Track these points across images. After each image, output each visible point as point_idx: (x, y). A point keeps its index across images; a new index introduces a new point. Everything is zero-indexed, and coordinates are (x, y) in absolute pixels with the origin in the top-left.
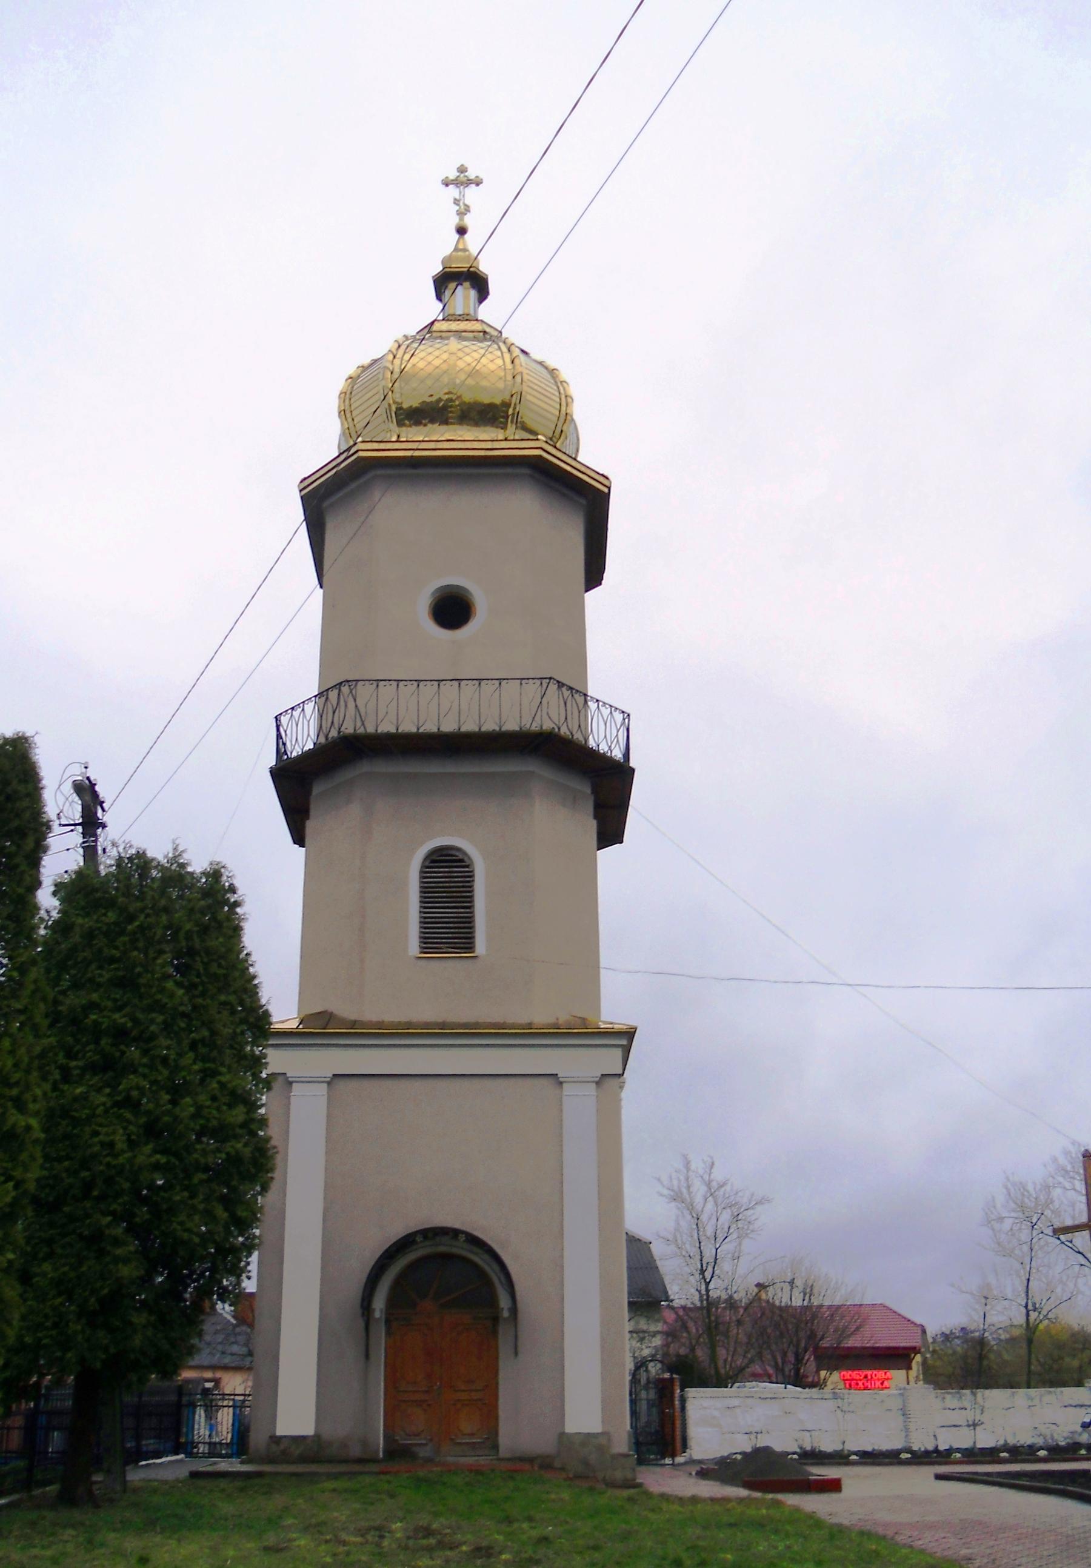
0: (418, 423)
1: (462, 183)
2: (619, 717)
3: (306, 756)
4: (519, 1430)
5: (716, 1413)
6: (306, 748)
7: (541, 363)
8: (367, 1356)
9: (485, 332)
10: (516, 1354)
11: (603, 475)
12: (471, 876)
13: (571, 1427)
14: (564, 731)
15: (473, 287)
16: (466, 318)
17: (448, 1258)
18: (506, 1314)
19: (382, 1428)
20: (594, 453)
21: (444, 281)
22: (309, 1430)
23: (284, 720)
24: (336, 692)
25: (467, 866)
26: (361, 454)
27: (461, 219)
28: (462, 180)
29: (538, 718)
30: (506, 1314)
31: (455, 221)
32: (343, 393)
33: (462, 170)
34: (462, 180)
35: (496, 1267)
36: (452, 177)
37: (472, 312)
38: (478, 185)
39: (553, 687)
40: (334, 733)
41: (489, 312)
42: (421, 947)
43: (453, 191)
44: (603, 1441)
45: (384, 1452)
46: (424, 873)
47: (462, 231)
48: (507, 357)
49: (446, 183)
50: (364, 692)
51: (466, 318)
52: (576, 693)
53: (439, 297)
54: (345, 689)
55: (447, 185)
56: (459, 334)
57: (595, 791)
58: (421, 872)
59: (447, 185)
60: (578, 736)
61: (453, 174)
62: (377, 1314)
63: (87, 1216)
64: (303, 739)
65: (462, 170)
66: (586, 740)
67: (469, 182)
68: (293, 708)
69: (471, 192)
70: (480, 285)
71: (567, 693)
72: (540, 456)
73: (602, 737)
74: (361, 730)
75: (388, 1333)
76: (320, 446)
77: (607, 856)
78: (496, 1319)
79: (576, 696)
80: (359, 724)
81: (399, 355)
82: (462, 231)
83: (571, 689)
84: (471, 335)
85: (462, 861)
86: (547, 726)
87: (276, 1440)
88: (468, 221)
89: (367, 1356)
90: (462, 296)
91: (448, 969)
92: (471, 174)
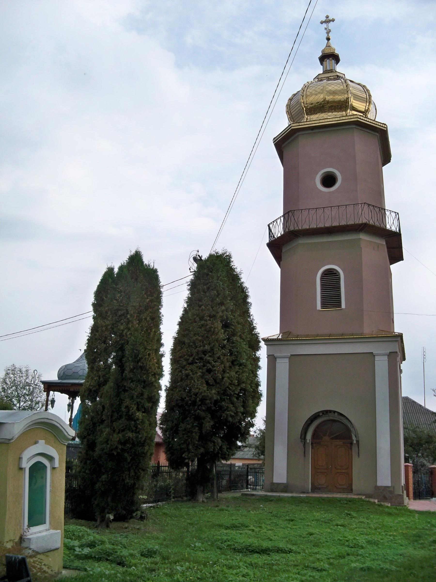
0: (340, 101)
1: (327, 22)
2: (393, 214)
3: (279, 238)
4: (359, 483)
6: (278, 236)
7: (359, 84)
8: (305, 456)
9: (338, 76)
10: (359, 456)
11: (383, 124)
13: (379, 484)
14: (371, 222)
15: (333, 59)
16: (331, 71)
17: (334, 421)
18: (355, 442)
19: (310, 484)
20: (381, 116)
21: (322, 59)
22: (286, 482)
23: (271, 226)
24: (287, 215)
25: (336, 274)
26: (292, 128)
27: (328, 35)
28: (328, 21)
29: (361, 219)
30: (355, 442)
32: (287, 105)
33: (327, 17)
34: (328, 21)
35: (347, 421)
36: (324, 20)
37: (333, 69)
38: (333, 21)
39: (366, 206)
40: (287, 230)
42: (321, 307)
43: (325, 25)
44: (391, 489)
45: (311, 489)
46: (321, 279)
48: (345, 85)
49: (322, 23)
51: (331, 71)
52: (382, 210)
53: (322, 64)
54: (290, 214)
55: (322, 24)
56: (328, 79)
57: (387, 243)
58: (321, 279)
59: (322, 24)
60: (382, 226)
61: (324, 19)
62: (308, 441)
63: (239, 568)
64: (279, 231)
65: (327, 17)
66: (386, 226)
67: (330, 21)
68: (273, 222)
69: (331, 25)
70: (336, 58)
71: (372, 208)
72: (358, 121)
73: (391, 224)
74: (297, 228)
75: (312, 448)
76: (281, 124)
78: (352, 444)
79: (376, 209)
81: (306, 90)
82: (328, 39)
83: (374, 206)
84: (332, 77)
85: (336, 274)
86: (365, 221)
87: (273, 484)
89: (305, 456)
90: (329, 63)
91: (332, 312)
92: (330, 18)
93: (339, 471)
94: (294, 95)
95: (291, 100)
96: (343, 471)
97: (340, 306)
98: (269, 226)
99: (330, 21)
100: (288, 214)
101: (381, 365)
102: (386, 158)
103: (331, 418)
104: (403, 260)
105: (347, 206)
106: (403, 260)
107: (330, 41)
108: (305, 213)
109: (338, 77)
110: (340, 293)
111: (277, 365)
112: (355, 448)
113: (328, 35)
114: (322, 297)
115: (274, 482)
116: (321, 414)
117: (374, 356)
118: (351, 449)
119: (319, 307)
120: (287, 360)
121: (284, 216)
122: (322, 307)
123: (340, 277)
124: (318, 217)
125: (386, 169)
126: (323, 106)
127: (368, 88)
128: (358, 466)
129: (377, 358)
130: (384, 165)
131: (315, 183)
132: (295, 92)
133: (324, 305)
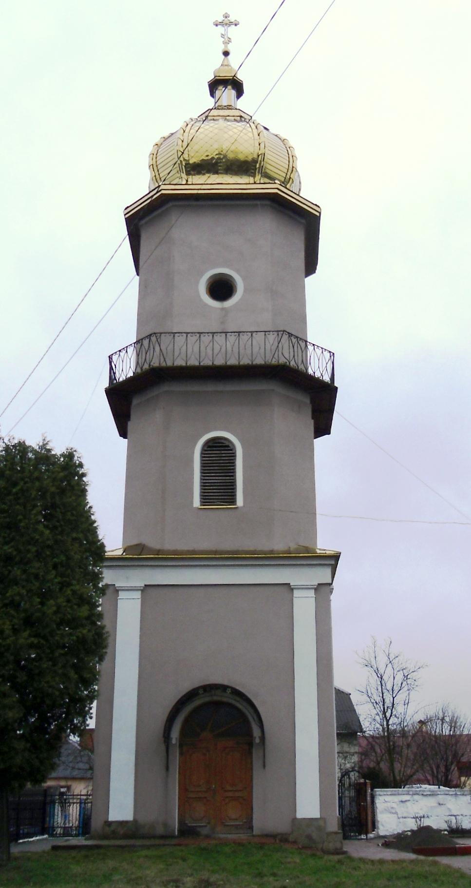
0: (199, 173)
2: (327, 355)
3: (129, 381)
4: (266, 818)
5: (394, 805)
6: (129, 376)
10: (264, 766)
12: (234, 456)
18: (257, 740)
20: (309, 190)
21: (215, 85)
23: (115, 358)
24: (147, 340)
28: (226, 22)
29: (276, 356)
30: (257, 740)
31: (222, 48)
34: (226, 22)
39: (285, 337)
40: (146, 366)
41: (242, 104)
43: (221, 29)
44: (321, 823)
47: (226, 54)
50: (165, 340)
53: (212, 94)
54: (153, 339)
55: (217, 25)
57: (313, 402)
61: (220, 19)
62: (174, 741)
64: (126, 370)
65: (226, 16)
67: (230, 24)
70: (238, 87)
71: (294, 340)
74: (164, 364)
75: (181, 754)
76: (138, 188)
77: (320, 443)
80: (162, 360)
82: (226, 54)
86: (282, 361)
87: (108, 824)
88: (230, 48)
90: (227, 95)
91: (219, 515)
92: (232, 19)
93: (230, 794)
94: (165, 139)
95: (154, 155)
96: (237, 794)
97: (233, 501)
98: (110, 358)
99: (230, 24)
100: (145, 342)
101: (304, 606)
102: (311, 266)
103: (215, 698)
104: (329, 433)
105: (254, 334)
106: (329, 433)
107: (229, 57)
108: (180, 340)
109: (241, 118)
110: (235, 479)
111: (120, 603)
112: (256, 754)
113: (226, 47)
114: (203, 485)
115: (110, 820)
116: (201, 691)
117: (292, 589)
118: (251, 753)
119: (197, 502)
120: (138, 595)
121: (139, 342)
122: (203, 503)
123: (235, 453)
124: (203, 348)
125: (310, 282)
126: (216, 163)
127: (292, 143)
128: (262, 786)
129: (296, 593)
130: (306, 276)
131: (197, 291)
132: (166, 134)
133: (205, 499)
